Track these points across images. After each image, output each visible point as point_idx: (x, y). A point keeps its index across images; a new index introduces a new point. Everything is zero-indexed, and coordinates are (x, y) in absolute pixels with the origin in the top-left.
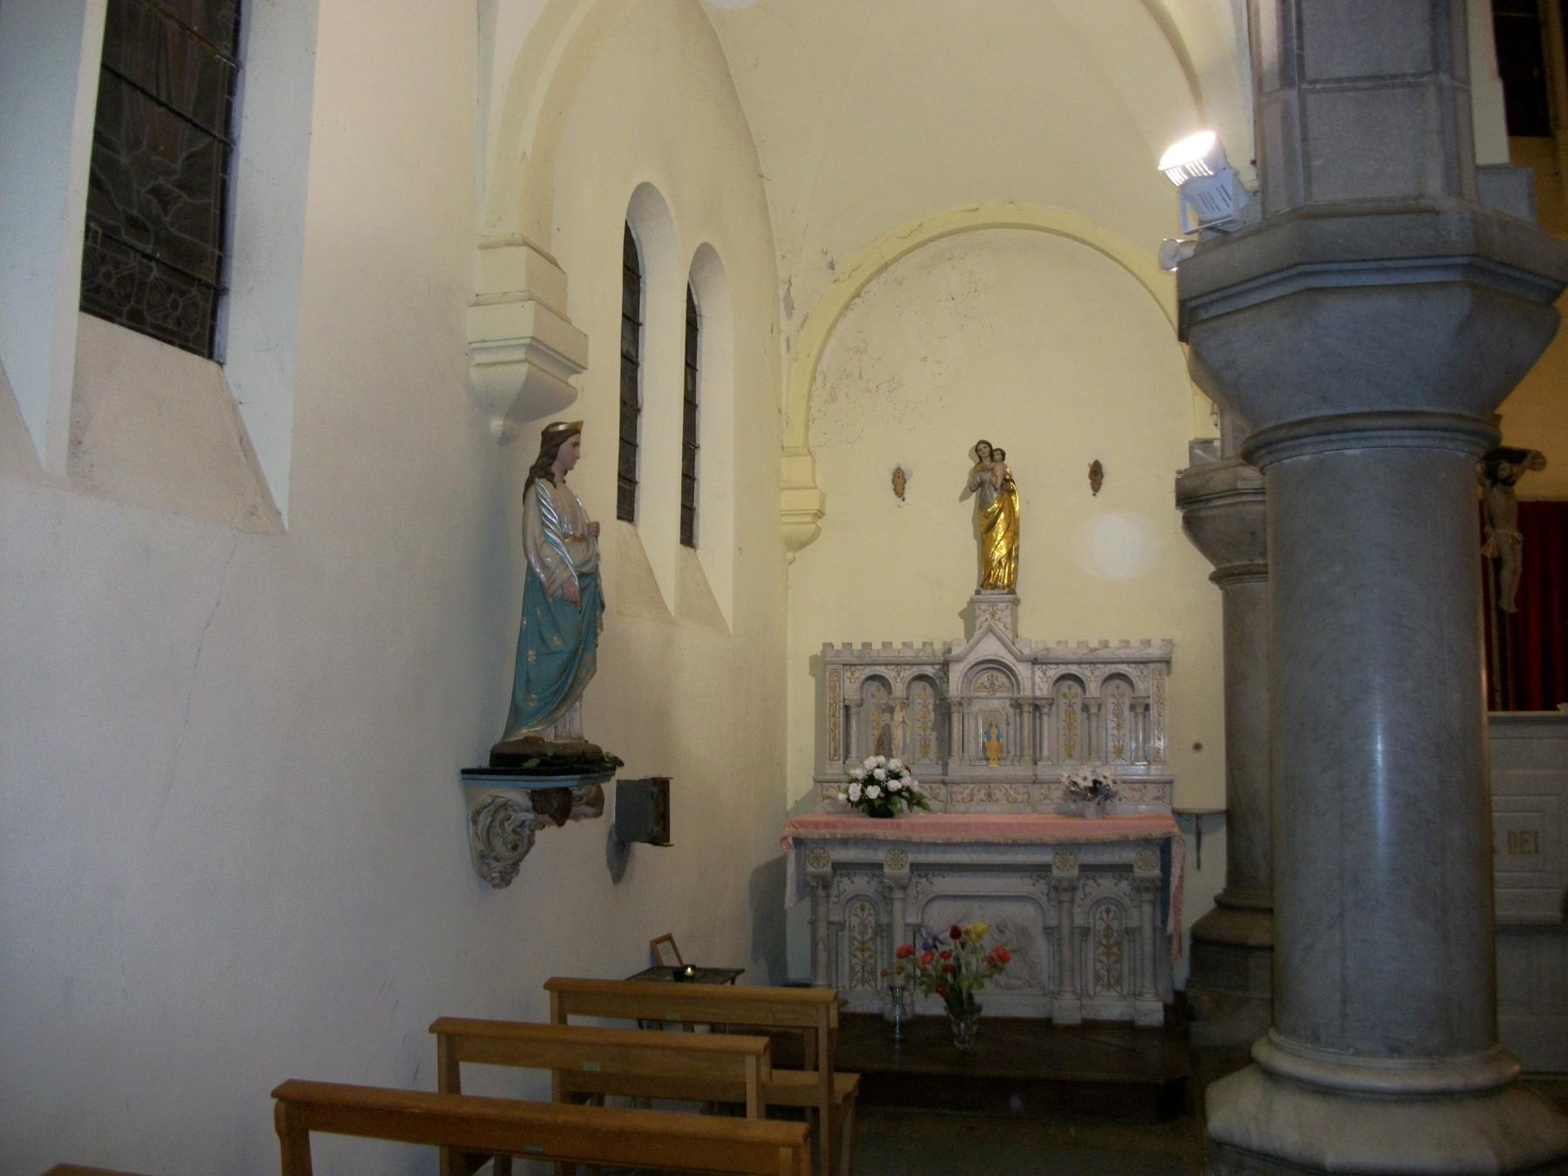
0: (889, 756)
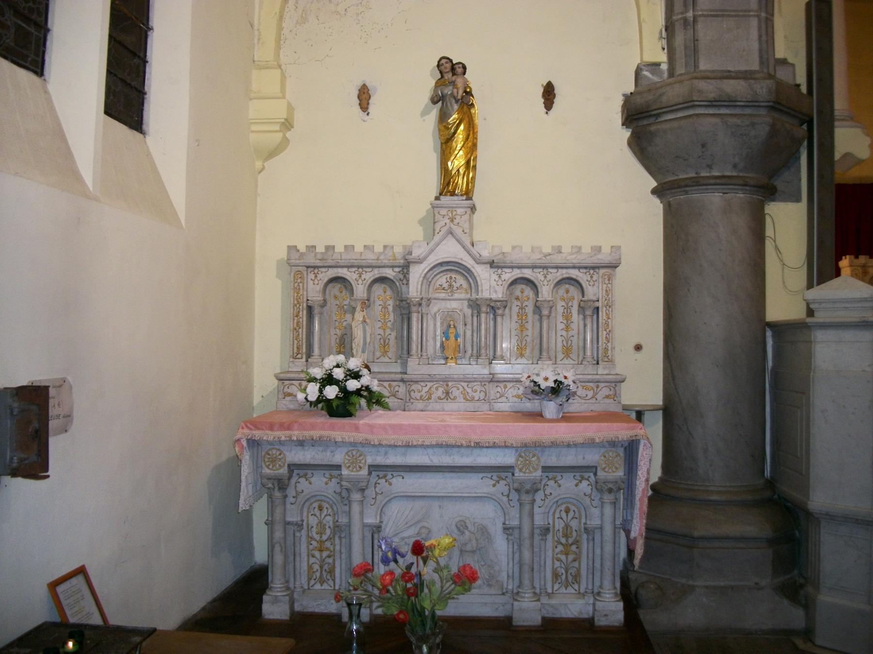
0: (349, 354)
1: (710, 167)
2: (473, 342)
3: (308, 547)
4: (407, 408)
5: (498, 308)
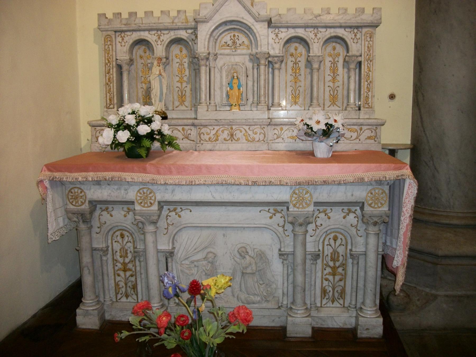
2: (253, 92)
3: (114, 268)
4: (197, 149)
5: (276, 63)
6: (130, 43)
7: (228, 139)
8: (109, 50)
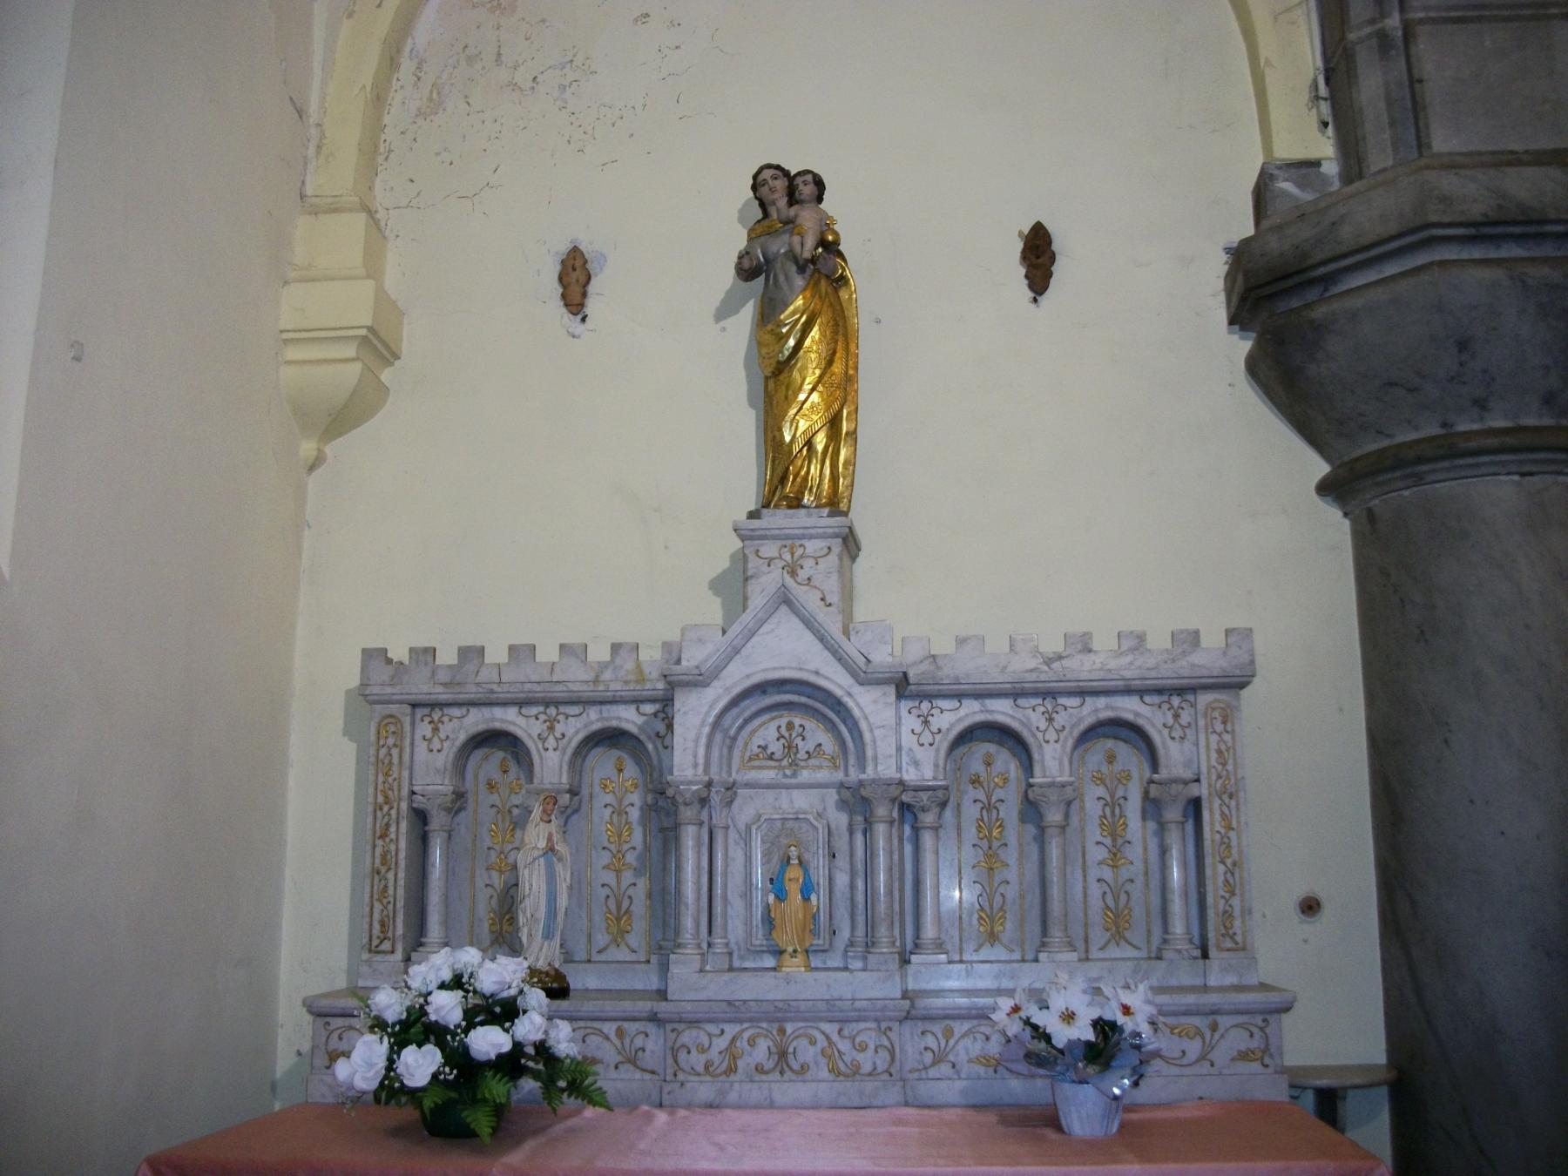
1: (1481, 404)
4: (666, 1100)
5: (923, 810)
6: (458, 743)
7: (769, 1065)
8: (391, 763)
